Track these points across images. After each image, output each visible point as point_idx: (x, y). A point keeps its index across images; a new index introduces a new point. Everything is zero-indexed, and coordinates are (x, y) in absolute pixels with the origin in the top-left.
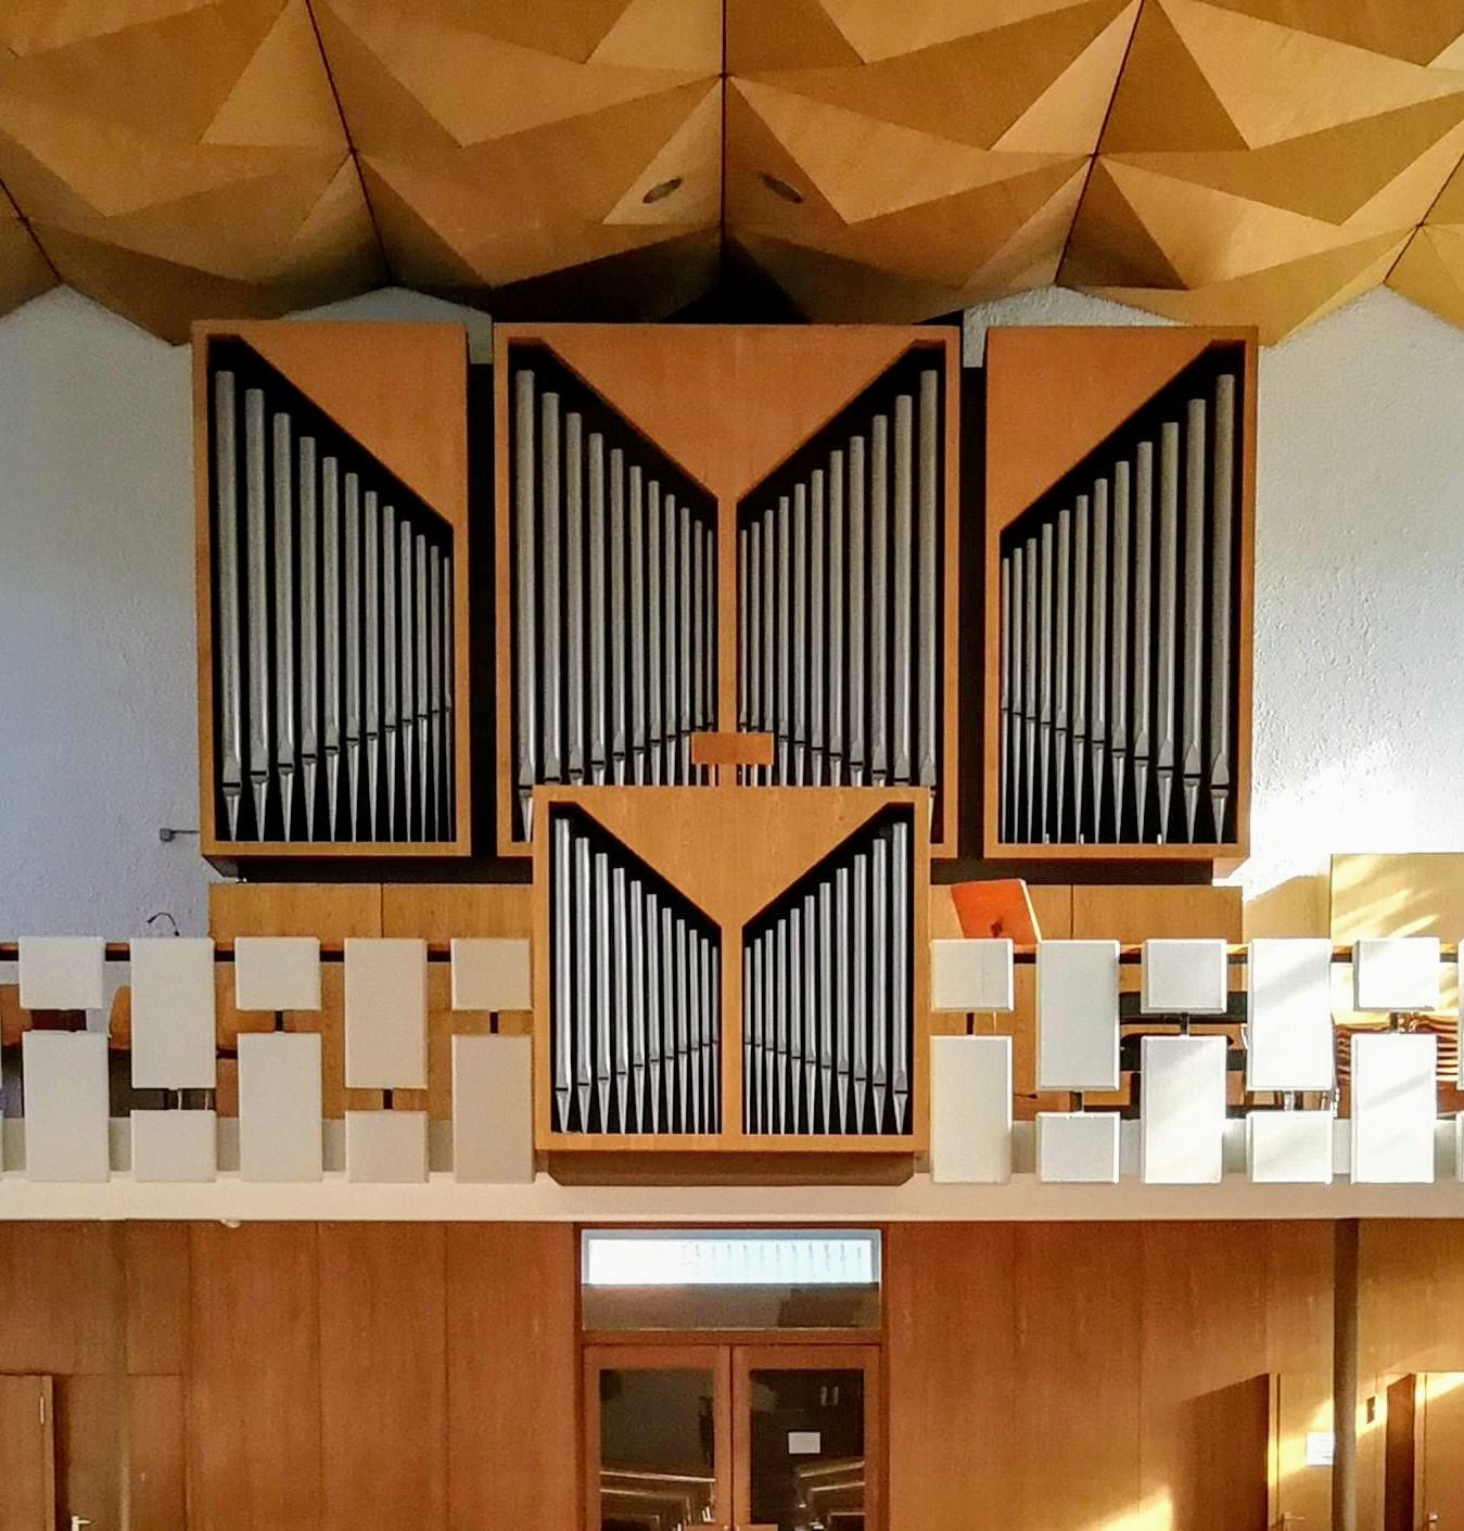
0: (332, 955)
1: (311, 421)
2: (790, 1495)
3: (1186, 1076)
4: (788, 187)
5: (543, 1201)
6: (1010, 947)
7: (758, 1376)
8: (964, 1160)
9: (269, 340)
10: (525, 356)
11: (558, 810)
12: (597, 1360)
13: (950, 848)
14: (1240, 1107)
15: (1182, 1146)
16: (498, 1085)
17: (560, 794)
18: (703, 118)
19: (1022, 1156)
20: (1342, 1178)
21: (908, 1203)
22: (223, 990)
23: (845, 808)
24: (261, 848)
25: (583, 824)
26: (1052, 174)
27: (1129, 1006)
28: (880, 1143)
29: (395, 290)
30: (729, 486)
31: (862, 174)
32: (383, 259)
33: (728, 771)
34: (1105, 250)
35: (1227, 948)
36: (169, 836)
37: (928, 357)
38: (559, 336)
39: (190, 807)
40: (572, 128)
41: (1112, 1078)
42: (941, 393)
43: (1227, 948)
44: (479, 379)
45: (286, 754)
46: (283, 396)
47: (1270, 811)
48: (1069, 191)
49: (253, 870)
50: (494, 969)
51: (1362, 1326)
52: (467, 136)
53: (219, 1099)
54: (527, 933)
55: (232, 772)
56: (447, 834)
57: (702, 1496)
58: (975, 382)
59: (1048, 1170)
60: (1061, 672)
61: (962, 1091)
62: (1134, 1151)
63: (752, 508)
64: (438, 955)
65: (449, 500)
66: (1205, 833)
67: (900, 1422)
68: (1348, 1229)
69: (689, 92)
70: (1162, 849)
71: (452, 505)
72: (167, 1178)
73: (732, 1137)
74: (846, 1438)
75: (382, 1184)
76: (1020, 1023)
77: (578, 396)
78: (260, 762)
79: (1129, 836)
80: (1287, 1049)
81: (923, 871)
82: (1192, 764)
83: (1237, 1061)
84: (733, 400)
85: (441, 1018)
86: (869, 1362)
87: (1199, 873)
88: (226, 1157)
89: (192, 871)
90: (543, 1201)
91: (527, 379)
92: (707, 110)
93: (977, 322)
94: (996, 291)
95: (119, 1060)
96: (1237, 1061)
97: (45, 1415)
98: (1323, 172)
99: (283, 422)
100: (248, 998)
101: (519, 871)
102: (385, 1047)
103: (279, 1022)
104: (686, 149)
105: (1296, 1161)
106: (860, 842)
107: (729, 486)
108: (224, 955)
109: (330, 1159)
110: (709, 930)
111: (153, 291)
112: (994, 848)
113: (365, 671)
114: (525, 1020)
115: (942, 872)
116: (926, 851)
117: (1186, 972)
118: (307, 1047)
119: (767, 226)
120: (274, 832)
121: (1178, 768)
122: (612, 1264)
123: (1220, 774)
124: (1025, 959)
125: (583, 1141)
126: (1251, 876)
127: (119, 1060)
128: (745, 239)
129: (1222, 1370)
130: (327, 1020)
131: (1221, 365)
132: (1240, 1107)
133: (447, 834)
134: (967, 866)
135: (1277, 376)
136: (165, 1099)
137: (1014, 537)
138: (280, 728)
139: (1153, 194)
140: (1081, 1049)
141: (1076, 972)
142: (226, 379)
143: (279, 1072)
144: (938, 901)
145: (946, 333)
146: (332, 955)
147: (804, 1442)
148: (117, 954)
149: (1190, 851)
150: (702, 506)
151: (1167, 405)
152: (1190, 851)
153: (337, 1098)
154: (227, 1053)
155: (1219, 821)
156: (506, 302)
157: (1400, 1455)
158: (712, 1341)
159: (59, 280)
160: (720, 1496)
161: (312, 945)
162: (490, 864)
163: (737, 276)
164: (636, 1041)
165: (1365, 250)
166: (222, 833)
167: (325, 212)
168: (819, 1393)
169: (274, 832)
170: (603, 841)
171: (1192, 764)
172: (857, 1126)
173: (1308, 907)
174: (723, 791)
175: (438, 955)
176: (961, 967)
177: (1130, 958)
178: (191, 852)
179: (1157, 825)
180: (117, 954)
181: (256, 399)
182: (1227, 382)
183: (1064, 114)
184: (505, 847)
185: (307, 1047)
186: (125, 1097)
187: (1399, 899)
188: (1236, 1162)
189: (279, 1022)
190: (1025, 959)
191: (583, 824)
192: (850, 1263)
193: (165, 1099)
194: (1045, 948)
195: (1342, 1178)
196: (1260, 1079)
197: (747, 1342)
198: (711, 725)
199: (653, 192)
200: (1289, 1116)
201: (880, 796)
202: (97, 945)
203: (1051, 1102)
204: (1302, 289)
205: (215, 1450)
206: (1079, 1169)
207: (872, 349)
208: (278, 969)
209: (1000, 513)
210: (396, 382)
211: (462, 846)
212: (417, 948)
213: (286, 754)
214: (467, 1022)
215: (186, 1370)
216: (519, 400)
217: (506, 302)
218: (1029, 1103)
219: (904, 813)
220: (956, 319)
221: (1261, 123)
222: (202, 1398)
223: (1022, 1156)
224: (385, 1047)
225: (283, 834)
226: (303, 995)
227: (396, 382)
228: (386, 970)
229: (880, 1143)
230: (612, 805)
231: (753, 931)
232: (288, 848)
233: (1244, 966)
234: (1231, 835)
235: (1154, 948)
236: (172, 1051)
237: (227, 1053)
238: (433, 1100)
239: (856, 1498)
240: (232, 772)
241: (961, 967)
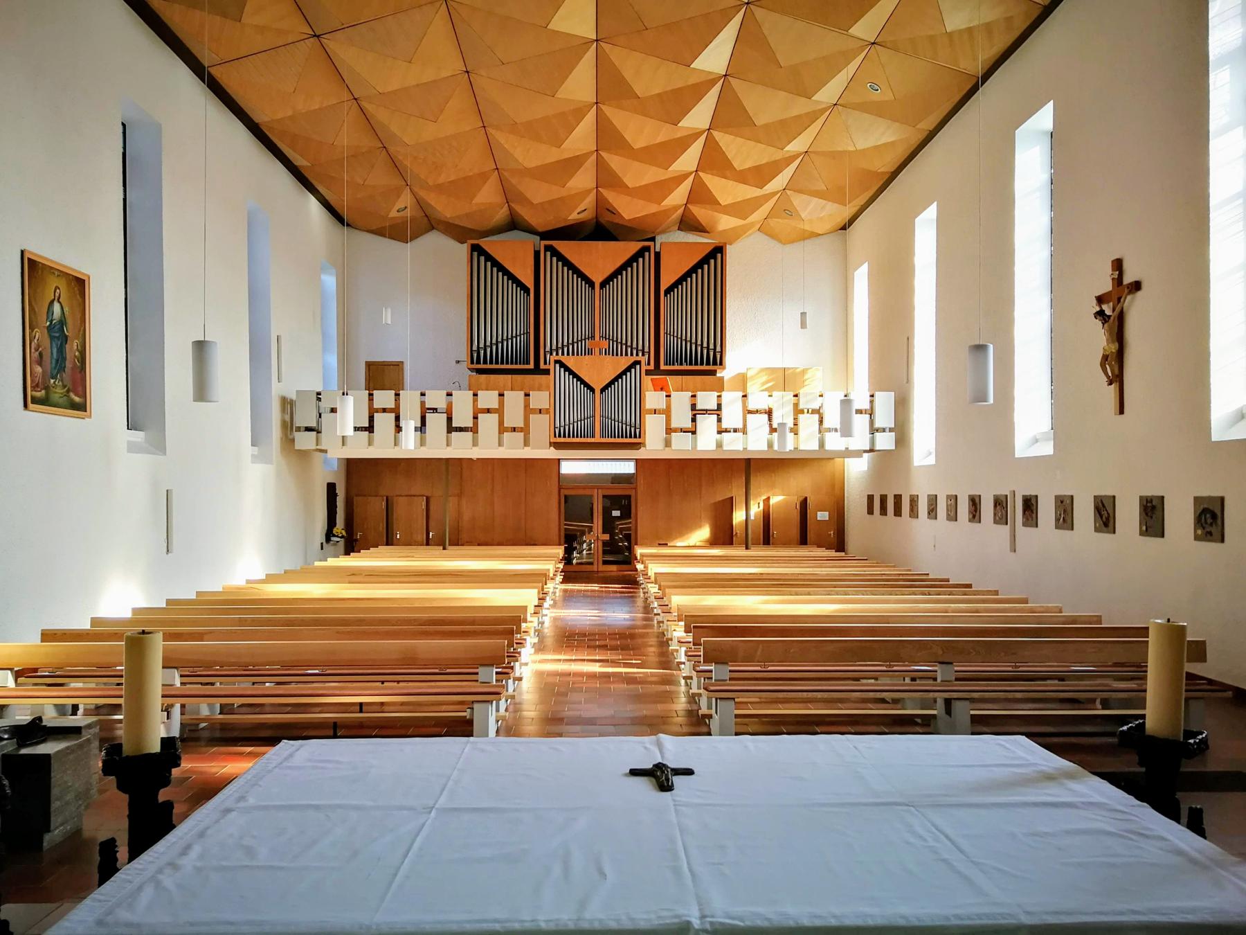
0: (501, 395)
1: (495, 263)
2: (614, 528)
3: (707, 425)
4: (613, 212)
5: (552, 453)
6: (665, 393)
7: (604, 496)
8: (654, 445)
9: (485, 243)
10: (547, 248)
11: (556, 362)
12: (564, 492)
13: (652, 367)
14: (719, 432)
15: (706, 442)
16: (541, 426)
17: (560, 357)
18: (591, 198)
19: (668, 443)
20: (745, 449)
21: (641, 454)
22: (475, 401)
23: (625, 362)
24: (482, 366)
25: (562, 365)
26: (676, 208)
27: (693, 407)
28: (633, 440)
29: (516, 232)
30: (598, 279)
31: (629, 209)
32: (514, 224)
33: (597, 350)
34: (688, 223)
35: (717, 394)
36: (458, 362)
37: (647, 249)
38: (555, 243)
39: (464, 355)
40: (562, 199)
41: (689, 425)
42: (649, 258)
43: (717, 394)
44: (537, 254)
45: (488, 343)
46: (489, 258)
47: (729, 358)
48: (680, 211)
49: (480, 371)
50: (540, 399)
51: (752, 487)
52: (535, 202)
53: (474, 429)
54: (548, 389)
55: (475, 348)
56: (528, 363)
57: (591, 529)
58: (658, 255)
59: (674, 446)
60: (680, 323)
61: (653, 428)
62: (695, 442)
63: (604, 284)
64: (527, 395)
65: (529, 282)
66: (715, 363)
67: (640, 509)
68: (748, 462)
69: (589, 191)
70: (705, 367)
71: (530, 284)
72: (462, 448)
73: (597, 439)
74: (627, 513)
75: (513, 449)
76: (667, 412)
77: (561, 258)
78: (482, 345)
79: (696, 364)
80: (732, 417)
81: (643, 372)
82: (712, 346)
83: (719, 420)
84: (598, 259)
85: (528, 410)
86: (632, 493)
87: (713, 373)
88: (475, 443)
89: (464, 372)
90: (552, 453)
91: (548, 254)
92: (591, 117)
93: (659, 239)
94: (663, 232)
95: (450, 419)
96: (719, 420)
97: (424, 507)
98: (741, 209)
99: (489, 264)
100: (481, 405)
101: (547, 372)
102: (514, 416)
103: (488, 411)
104: (589, 202)
105: (734, 445)
106: (628, 369)
107: (598, 279)
108: (475, 395)
109: (500, 444)
110: (592, 390)
111: (457, 232)
112: (663, 367)
113: (509, 325)
114: (547, 411)
115: (648, 373)
116: (644, 368)
117: (707, 400)
118: (494, 418)
119: (606, 218)
120: (485, 362)
121: (708, 347)
122: (567, 468)
123: (718, 349)
124: (668, 396)
125: (562, 440)
126: (727, 373)
127: (450, 419)
128: (602, 220)
129: (721, 496)
130: (500, 411)
131: (717, 252)
132: (719, 432)
133: (528, 363)
134: (657, 370)
135: (730, 251)
136: (461, 429)
137: (668, 291)
138: (487, 336)
139: (699, 212)
140: (681, 418)
141: (681, 400)
142: (475, 254)
143: (488, 423)
144: (647, 380)
145: (651, 244)
146: (501, 395)
147: (616, 513)
148: (449, 394)
149: (711, 367)
150: (591, 284)
151: (705, 261)
152: (711, 367)
153: (502, 429)
154: (475, 418)
155: (717, 360)
156: (545, 235)
157: (766, 516)
158: (593, 488)
159: (433, 228)
160: (595, 529)
161: (497, 393)
162: (537, 370)
163: (600, 229)
164: (575, 416)
165: (752, 224)
166: (472, 362)
167: (501, 215)
168: (11, 786)
169: (485, 362)
170: (567, 369)
171: (712, 346)
172: (630, 438)
173: (742, 381)
174: (595, 358)
175: (527, 395)
176: (653, 399)
177: (694, 396)
178: (465, 365)
179: (702, 361)
180: (449, 394)
181: (482, 258)
182: (719, 255)
183: (678, 197)
184: (542, 366)
185: (494, 418)
186: (451, 429)
187: (764, 378)
188: (719, 445)
189: (488, 411)
190: (668, 396)
191: (562, 365)
192: (629, 468)
193: (461, 429)
194: (673, 394)
195: (745, 449)
196: (724, 425)
197: (602, 488)
198: (593, 337)
199: (580, 212)
200: (732, 434)
201: (631, 360)
202: (445, 392)
203: (675, 430)
204: (736, 234)
205: (467, 516)
206: (682, 447)
207: (634, 247)
208: (488, 398)
209: (663, 288)
210: (516, 254)
211: (531, 366)
212: (522, 393)
213: (488, 343)
214: (534, 411)
215: (460, 495)
216: (546, 257)
217: (545, 235)
218: (669, 430)
219: (639, 363)
220: (653, 239)
221: (724, 200)
222: (464, 502)
223: (668, 443)
224: (514, 416)
225: (488, 363)
226: (494, 404)
227: (516, 254)
228: (514, 399)
229: (633, 440)
230: (570, 362)
231: (603, 390)
232: (488, 366)
233: (548, 560)
234: (721, 364)
235: (699, 394)
236: (462, 418)
237: (475, 418)
238: (525, 430)
239: (629, 529)
240: (475, 348)
241: (653, 399)
